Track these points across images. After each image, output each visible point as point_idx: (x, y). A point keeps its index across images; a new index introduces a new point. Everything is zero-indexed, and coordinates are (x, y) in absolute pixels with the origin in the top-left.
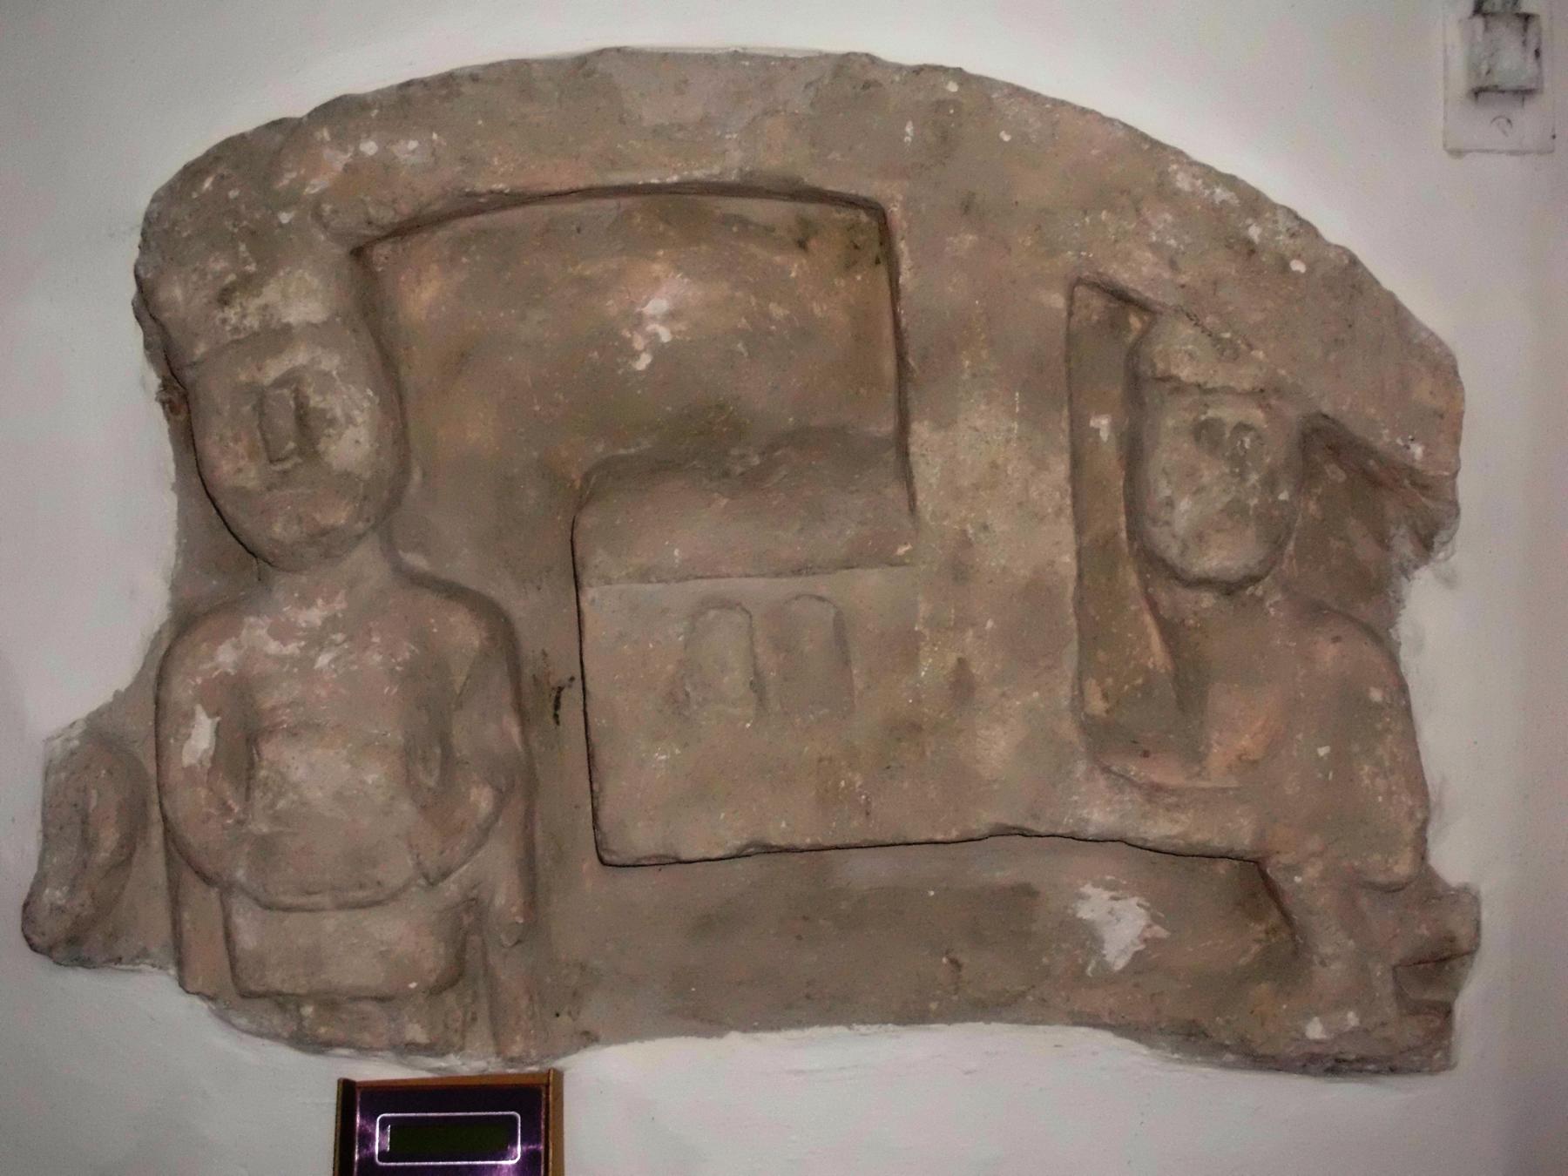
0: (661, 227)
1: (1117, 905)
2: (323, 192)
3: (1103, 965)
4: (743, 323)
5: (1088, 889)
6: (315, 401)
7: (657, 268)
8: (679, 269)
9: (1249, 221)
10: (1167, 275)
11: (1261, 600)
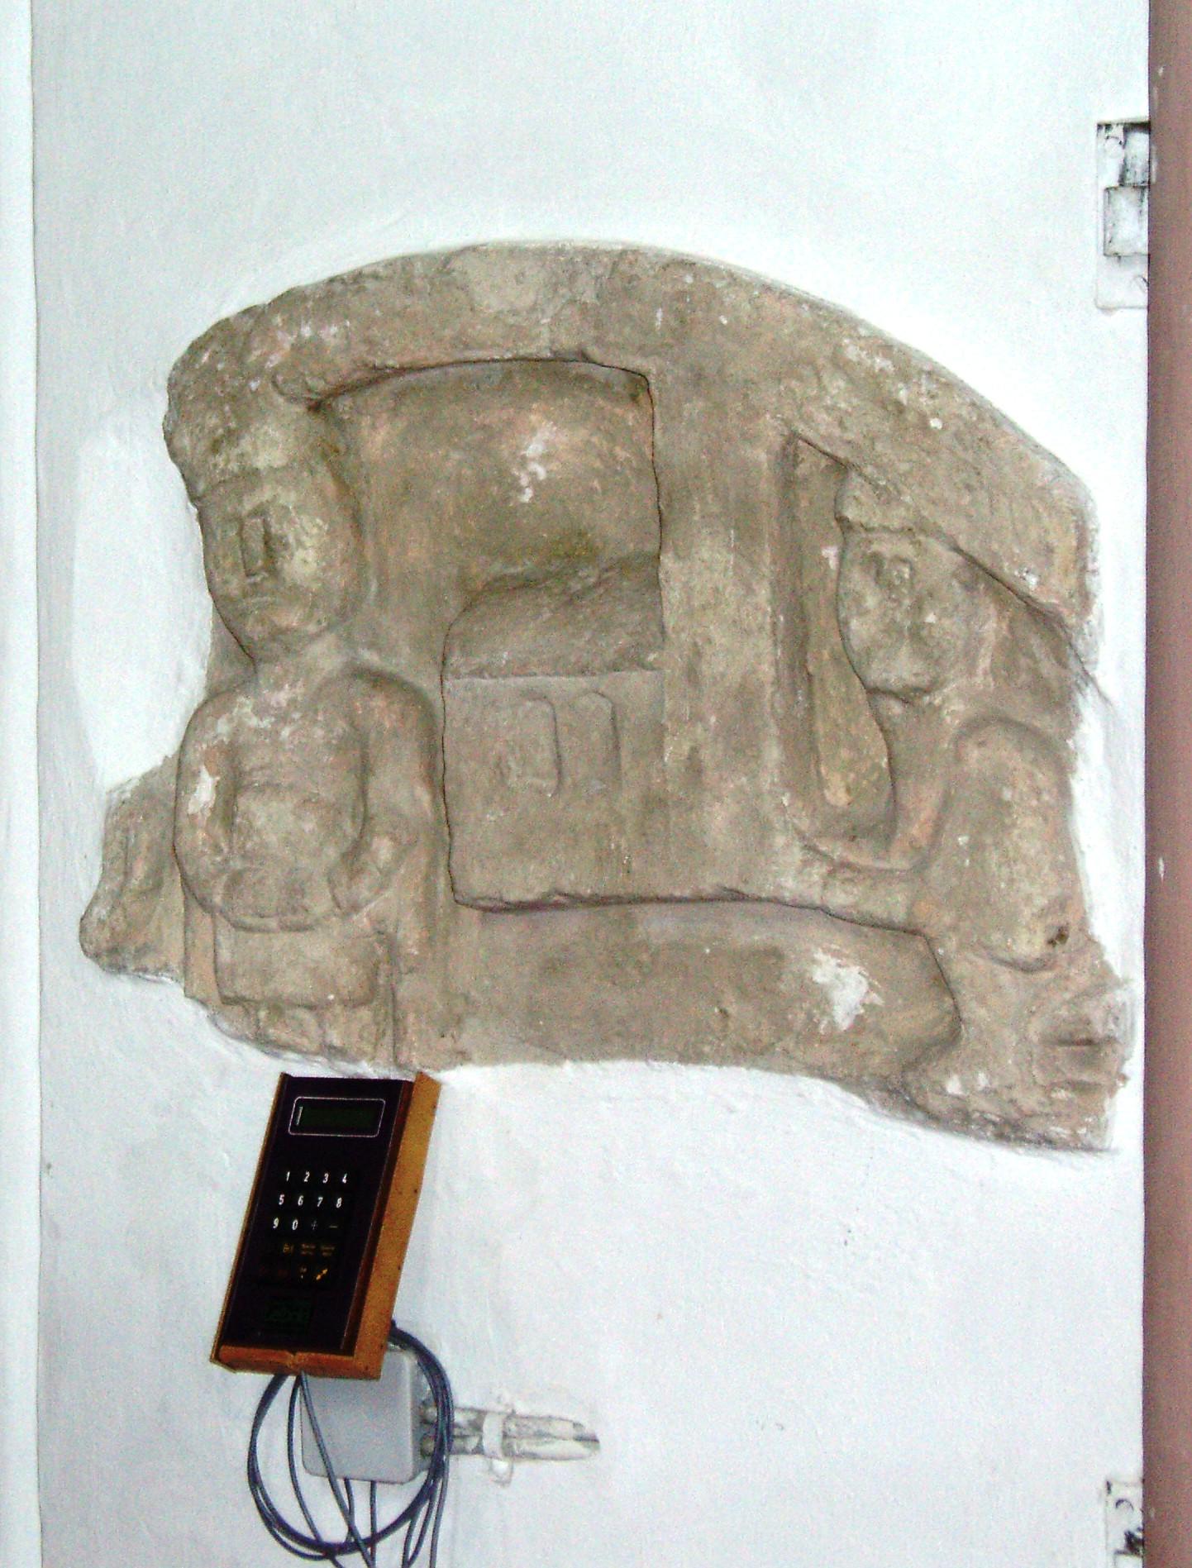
0: (535, 385)
1: (843, 972)
2: (281, 365)
3: (832, 1024)
4: (598, 464)
5: (819, 955)
6: (275, 529)
7: (533, 418)
8: (549, 419)
9: (900, 385)
10: (837, 432)
11: (940, 708)
